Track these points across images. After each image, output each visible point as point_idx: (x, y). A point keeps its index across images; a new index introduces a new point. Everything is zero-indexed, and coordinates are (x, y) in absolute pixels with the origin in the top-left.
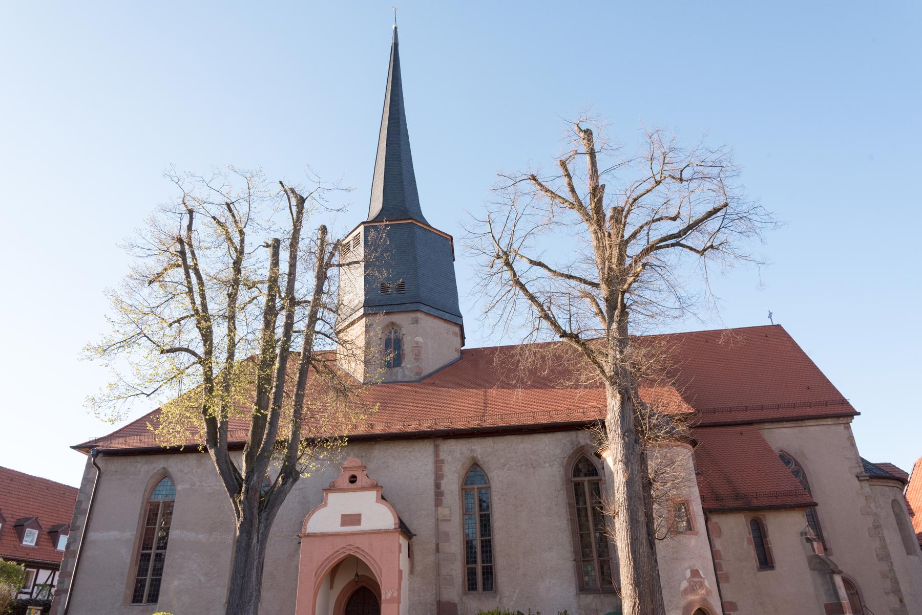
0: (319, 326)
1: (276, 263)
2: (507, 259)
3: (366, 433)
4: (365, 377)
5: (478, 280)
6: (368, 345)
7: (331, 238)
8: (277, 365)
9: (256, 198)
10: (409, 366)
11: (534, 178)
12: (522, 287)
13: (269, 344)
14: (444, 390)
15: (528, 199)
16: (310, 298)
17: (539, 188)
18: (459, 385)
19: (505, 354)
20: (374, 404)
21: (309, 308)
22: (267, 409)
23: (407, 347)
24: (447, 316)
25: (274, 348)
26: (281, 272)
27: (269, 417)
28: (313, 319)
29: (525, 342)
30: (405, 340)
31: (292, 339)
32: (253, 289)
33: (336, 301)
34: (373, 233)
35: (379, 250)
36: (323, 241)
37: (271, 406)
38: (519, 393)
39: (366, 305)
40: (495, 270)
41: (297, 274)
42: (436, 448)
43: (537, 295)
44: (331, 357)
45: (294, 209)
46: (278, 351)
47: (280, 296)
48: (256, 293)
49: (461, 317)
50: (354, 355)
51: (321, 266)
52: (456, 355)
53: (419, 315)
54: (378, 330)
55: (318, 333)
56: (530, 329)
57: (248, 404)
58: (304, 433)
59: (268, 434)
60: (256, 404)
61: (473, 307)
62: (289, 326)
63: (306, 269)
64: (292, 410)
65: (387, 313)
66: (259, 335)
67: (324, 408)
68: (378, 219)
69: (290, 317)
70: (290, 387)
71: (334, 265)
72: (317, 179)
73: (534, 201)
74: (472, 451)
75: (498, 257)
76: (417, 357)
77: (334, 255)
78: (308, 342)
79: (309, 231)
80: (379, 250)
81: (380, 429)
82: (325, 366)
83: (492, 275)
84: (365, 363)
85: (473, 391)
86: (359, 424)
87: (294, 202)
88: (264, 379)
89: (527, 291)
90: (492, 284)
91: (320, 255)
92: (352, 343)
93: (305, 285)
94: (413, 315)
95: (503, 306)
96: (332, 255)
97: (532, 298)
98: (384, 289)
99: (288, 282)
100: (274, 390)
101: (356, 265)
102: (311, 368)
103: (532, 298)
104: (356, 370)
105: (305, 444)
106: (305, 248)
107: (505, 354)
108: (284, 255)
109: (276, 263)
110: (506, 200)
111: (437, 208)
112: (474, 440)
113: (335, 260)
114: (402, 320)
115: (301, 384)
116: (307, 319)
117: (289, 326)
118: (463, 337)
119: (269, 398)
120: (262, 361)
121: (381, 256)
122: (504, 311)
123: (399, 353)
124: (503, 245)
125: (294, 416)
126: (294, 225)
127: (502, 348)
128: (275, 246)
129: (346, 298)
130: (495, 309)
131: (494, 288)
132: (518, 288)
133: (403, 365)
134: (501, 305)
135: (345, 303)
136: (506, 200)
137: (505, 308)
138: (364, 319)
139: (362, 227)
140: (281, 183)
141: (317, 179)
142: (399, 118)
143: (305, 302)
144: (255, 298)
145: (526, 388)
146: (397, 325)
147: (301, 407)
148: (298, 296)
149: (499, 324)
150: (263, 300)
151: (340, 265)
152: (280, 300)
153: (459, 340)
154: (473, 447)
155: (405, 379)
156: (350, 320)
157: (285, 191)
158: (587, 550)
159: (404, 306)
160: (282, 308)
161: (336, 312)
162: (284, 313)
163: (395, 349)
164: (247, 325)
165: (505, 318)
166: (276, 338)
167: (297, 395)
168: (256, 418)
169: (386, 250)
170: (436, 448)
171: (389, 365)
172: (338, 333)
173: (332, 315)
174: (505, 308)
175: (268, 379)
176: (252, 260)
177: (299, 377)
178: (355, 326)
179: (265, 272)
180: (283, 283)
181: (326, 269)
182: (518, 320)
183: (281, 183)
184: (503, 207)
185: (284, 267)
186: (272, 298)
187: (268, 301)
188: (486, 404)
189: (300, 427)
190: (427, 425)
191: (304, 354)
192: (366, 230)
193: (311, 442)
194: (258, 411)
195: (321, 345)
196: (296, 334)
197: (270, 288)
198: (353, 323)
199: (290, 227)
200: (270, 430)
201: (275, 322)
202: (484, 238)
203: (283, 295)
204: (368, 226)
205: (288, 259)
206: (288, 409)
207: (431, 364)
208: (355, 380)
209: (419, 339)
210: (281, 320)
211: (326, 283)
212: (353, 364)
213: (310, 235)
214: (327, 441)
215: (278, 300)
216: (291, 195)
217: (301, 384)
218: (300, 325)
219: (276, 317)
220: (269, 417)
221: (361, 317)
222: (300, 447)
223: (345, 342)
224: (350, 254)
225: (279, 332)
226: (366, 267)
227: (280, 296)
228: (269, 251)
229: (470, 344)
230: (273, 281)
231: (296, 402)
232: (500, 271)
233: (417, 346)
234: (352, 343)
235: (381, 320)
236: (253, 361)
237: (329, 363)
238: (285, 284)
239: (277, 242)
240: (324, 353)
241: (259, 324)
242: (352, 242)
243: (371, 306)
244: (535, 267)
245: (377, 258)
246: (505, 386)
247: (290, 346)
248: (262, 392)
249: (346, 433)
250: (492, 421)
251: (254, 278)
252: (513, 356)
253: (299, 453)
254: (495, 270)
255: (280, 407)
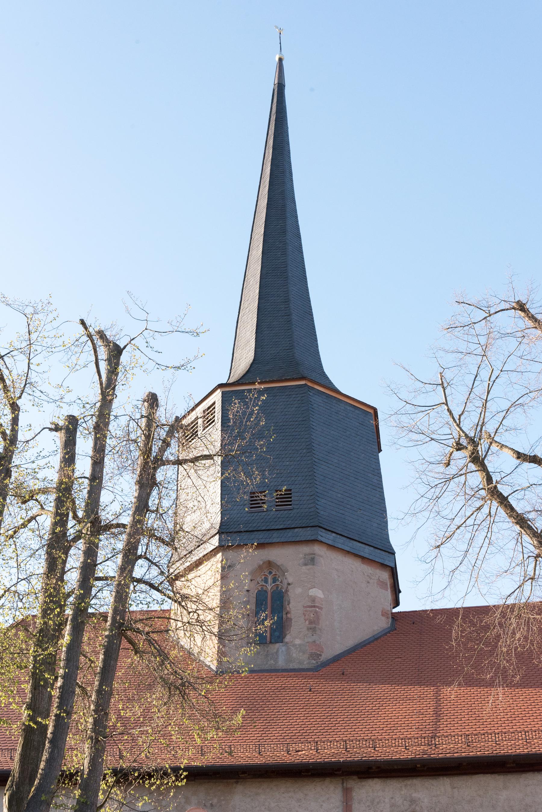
0: (140, 570)
1: (69, 458)
2: (474, 450)
3: (219, 762)
4: (220, 662)
5: (423, 489)
6: (225, 604)
7: (165, 414)
8: (66, 639)
9: (39, 349)
10: (298, 642)
11: (521, 307)
12: (504, 501)
13: (53, 598)
14: (361, 688)
15: (513, 343)
16: (126, 519)
17: (530, 324)
18: (392, 678)
19: (474, 625)
20: (235, 712)
21: (124, 537)
22: (47, 716)
23: (295, 607)
24: (366, 551)
25: (62, 607)
26: (77, 474)
27: (50, 730)
28: (130, 556)
29: (510, 601)
30: (291, 594)
31: (93, 592)
32: (31, 503)
33: (170, 526)
34: (236, 406)
35: (248, 435)
36: (150, 419)
37: (54, 711)
38: (499, 697)
39: (224, 530)
40: (453, 470)
41: (106, 478)
42: (347, 792)
43: (531, 516)
44: (159, 624)
45: (104, 366)
46: (69, 612)
47: (75, 517)
48: (35, 511)
49: (393, 553)
50: (200, 623)
51: (145, 466)
52: (384, 623)
53: (317, 549)
54: (244, 578)
55: (139, 581)
56: (518, 579)
57: (14, 706)
58: (110, 760)
59: (48, 761)
60: (29, 707)
61: (413, 538)
62: (88, 570)
63: (122, 468)
64: (91, 720)
65: (261, 546)
66: (38, 584)
67: (147, 713)
68: (247, 378)
69: (91, 553)
70: (89, 678)
71: (168, 462)
72: (144, 316)
73: (522, 347)
74: (413, 801)
75: (459, 447)
76: (313, 625)
77: (168, 445)
78: (121, 597)
79: (127, 403)
80: (248, 435)
81: (245, 756)
82: (150, 642)
83: (450, 480)
84: (221, 636)
85: (416, 691)
86: (205, 746)
87: (103, 353)
88: (44, 662)
89: (512, 509)
90: (448, 497)
91: (146, 445)
92: (198, 600)
93: (118, 496)
94: (305, 549)
95: (468, 536)
96: (166, 444)
97: (521, 521)
98: (255, 503)
99: (89, 492)
100: (59, 683)
101: (208, 462)
102: (125, 643)
103: (521, 521)
104: (207, 650)
105: (111, 780)
106: (119, 433)
107: (474, 625)
108: (84, 445)
109: (69, 458)
110: (473, 347)
111: (348, 362)
112: (417, 782)
113: (170, 454)
114: (286, 556)
115: (107, 673)
116: (120, 557)
117: (88, 570)
118: (396, 590)
119: (50, 697)
120: (41, 631)
121: (251, 443)
122: (470, 545)
123: (281, 618)
124: (468, 425)
125: (94, 730)
126: (103, 393)
127: (468, 611)
128: (70, 429)
129: (188, 519)
130: (453, 541)
131: (453, 503)
132: (495, 504)
133: (288, 639)
134: (464, 534)
135: (186, 528)
136: (473, 347)
137: (472, 539)
138: (219, 556)
139: (219, 393)
140: (83, 322)
141: (144, 316)
142: (284, 206)
143: (118, 525)
144: (33, 518)
145: (510, 685)
146: (278, 567)
147: (106, 714)
148: (106, 515)
149: (462, 568)
150: (46, 521)
151: (179, 462)
152: (75, 521)
153: (388, 594)
154: (415, 795)
155: (291, 666)
156: (195, 558)
157: (90, 336)
158: (113, 377)
159: (290, 533)
160: (77, 538)
161: (170, 543)
162: (81, 544)
163: (273, 612)
164: (19, 566)
165: (471, 557)
166: (67, 589)
167: (99, 692)
168: (28, 731)
169: (260, 436)
170: (347, 792)
171: (262, 640)
172: (172, 581)
173: (164, 550)
174: (472, 539)
175: (50, 663)
176: (31, 454)
177: (105, 661)
178: (203, 568)
179: (51, 475)
180: (81, 494)
181: (155, 469)
182: (497, 561)
183: (83, 322)
184: (468, 358)
185: (83, 466)
186: (60, 520)
187: (55, 524)
188: (438, 714)
189: (104, 750)
190: (330, 752)
191: (114, 618)
192: (226, 400)
193: (122, 777)
194: (32, 718)
195: (141, 601)
196: (99, 584)
197: (59, 502)
198: (199, 563)
199: (94, 395)
200: (51, 754)
201: (64, 562)
202: (432, 414)
203: (80, 514)
204: (230, 391)
205: (91, 452)
206: (84, 717)
207: (337, 640)
208: (202, 664)
209: (317, 593)
210: (75, 559)
211: (155, 493)
212: (198, 639)
213: (129, 409)
214: (150, 776)
215: (71, 523)
216: (99, 343)
217: (107, 673)
218: (109, 568)
219: (66, 553)
220: (50, 730)
221: (214, 552)
222: (103, 786)
223: (185, 597)
224: (195, 442)
225: (72, 578)
226: (224, 466)
227: (75, 517)
228: (59, 438)
229: (408, 603)
230: (65, 490)
231: (97, 705)
232: (462, 473)
233: (313, 605)
234: (198, 600)
235: (249, 557)
236: (27, 630)
237: (155, 636)
238: (85, 493)
239: (73, 423)
240: (149, 616)
241: (38, 566)
242: (200, 421)
243: (233, 532)
244: (527, 465)
245: (243, 451)
246: (470, 682)
247: (89, 605)
248: (39, 687)
249: (184, 763)
250: (449, 747)
251: (33, 484)
252: (487, 628)
253: (101, 797)
254: (453, 470)
255: (69, 714)
